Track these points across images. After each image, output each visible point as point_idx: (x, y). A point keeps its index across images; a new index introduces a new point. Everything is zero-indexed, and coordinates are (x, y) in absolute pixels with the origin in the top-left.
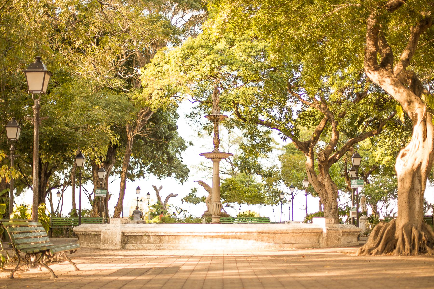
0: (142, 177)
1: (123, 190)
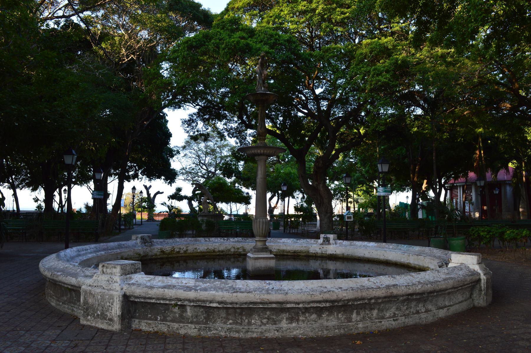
0: (136, 179)
1: (121, 188)
